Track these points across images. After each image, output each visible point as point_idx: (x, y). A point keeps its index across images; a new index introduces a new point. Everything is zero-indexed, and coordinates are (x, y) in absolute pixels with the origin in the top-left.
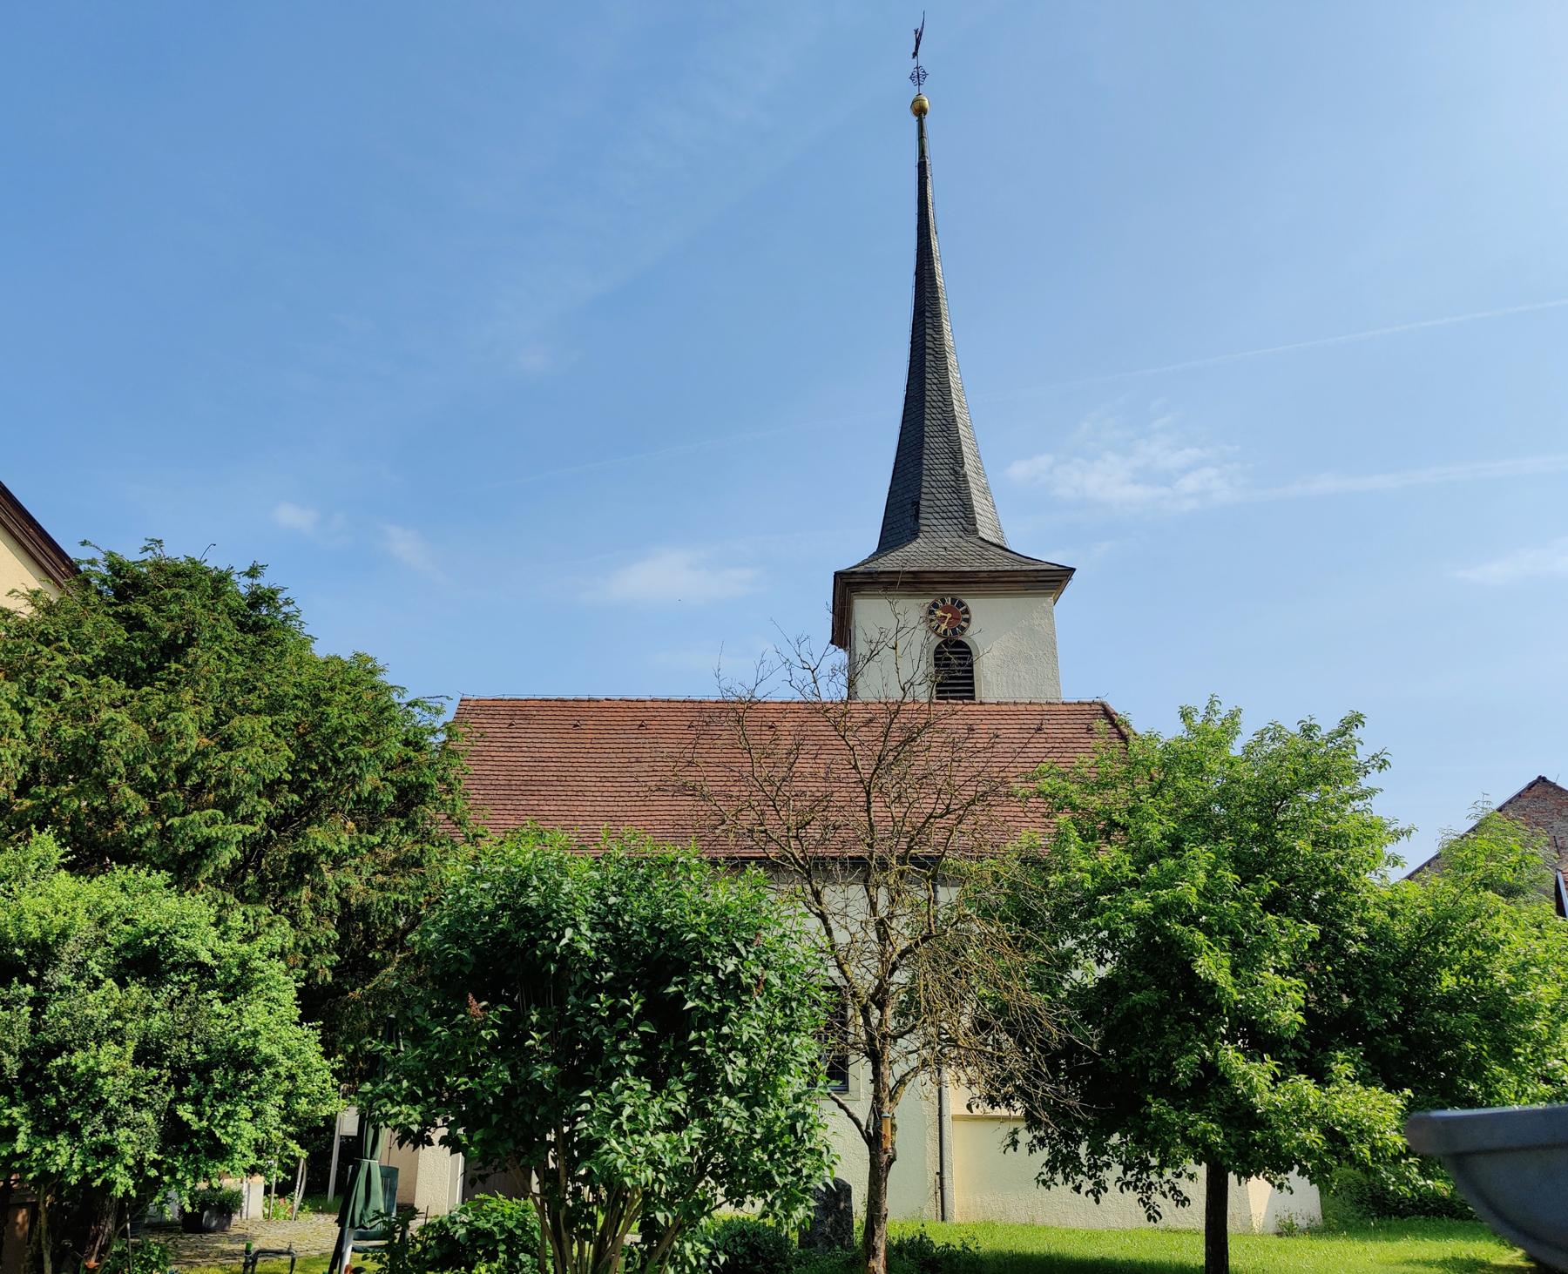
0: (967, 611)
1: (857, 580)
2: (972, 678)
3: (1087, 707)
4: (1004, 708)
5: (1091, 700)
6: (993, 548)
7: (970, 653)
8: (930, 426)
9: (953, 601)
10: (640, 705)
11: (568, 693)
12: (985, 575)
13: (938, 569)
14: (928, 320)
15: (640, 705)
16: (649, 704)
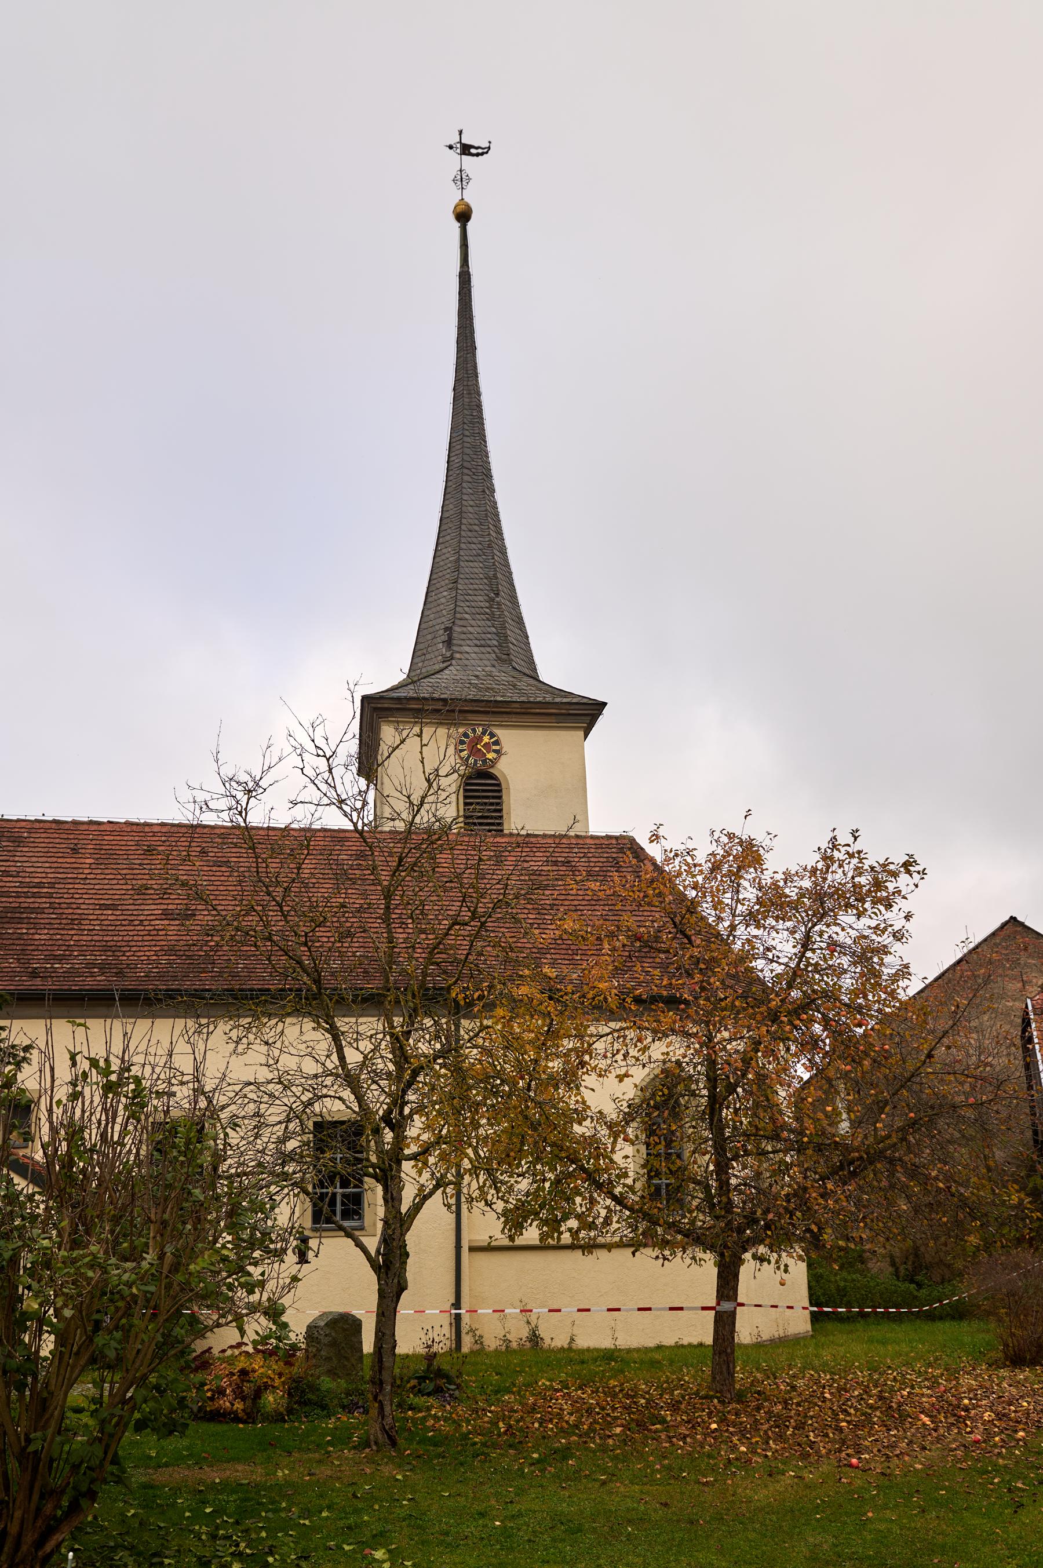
1: (386, 706)
7: (499, 785)
11: (66, 814)
12: (517, 705)
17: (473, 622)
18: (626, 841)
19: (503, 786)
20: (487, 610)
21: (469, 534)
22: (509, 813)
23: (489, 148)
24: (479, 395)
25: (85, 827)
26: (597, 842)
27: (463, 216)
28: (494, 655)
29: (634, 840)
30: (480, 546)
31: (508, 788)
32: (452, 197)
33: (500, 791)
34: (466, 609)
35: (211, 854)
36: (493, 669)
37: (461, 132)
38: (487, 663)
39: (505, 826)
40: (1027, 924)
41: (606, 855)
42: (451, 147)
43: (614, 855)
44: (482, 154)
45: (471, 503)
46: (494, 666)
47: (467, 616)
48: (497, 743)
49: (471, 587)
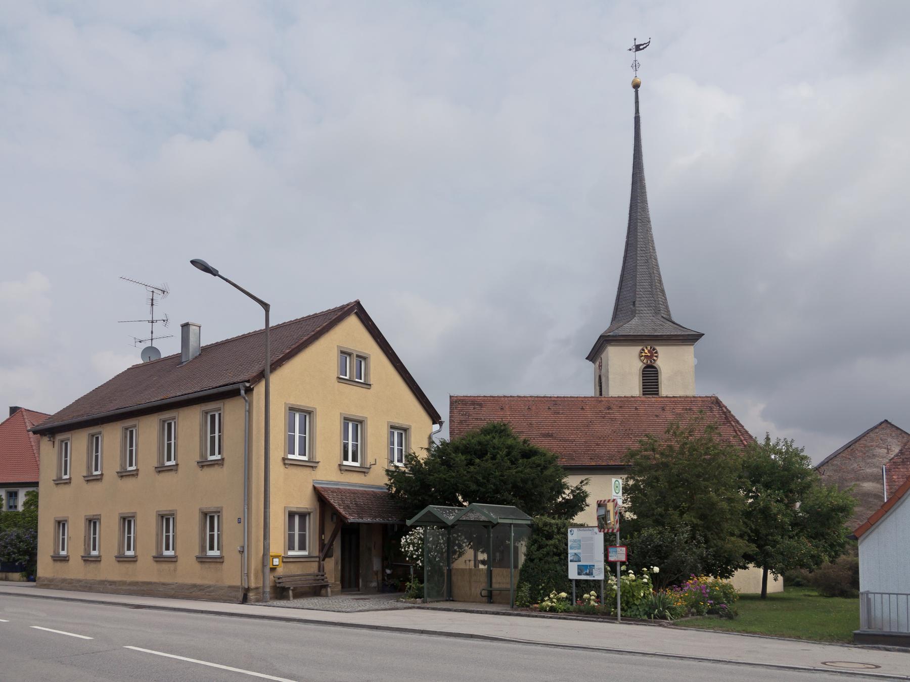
7: (657, 371)
23: (649, 42)
24: (649, 222)
27: (636, 86)
29: (718, 398)
32: (630, 77)
33: (657, 374)
36: (653, 318)
37: (635, 40)
39: (660, 394)
40: (892, 423)
41: (706, 405)
42: (630, 50)
44: (648, 45)
45: (642, 237)
48: (656, 353)
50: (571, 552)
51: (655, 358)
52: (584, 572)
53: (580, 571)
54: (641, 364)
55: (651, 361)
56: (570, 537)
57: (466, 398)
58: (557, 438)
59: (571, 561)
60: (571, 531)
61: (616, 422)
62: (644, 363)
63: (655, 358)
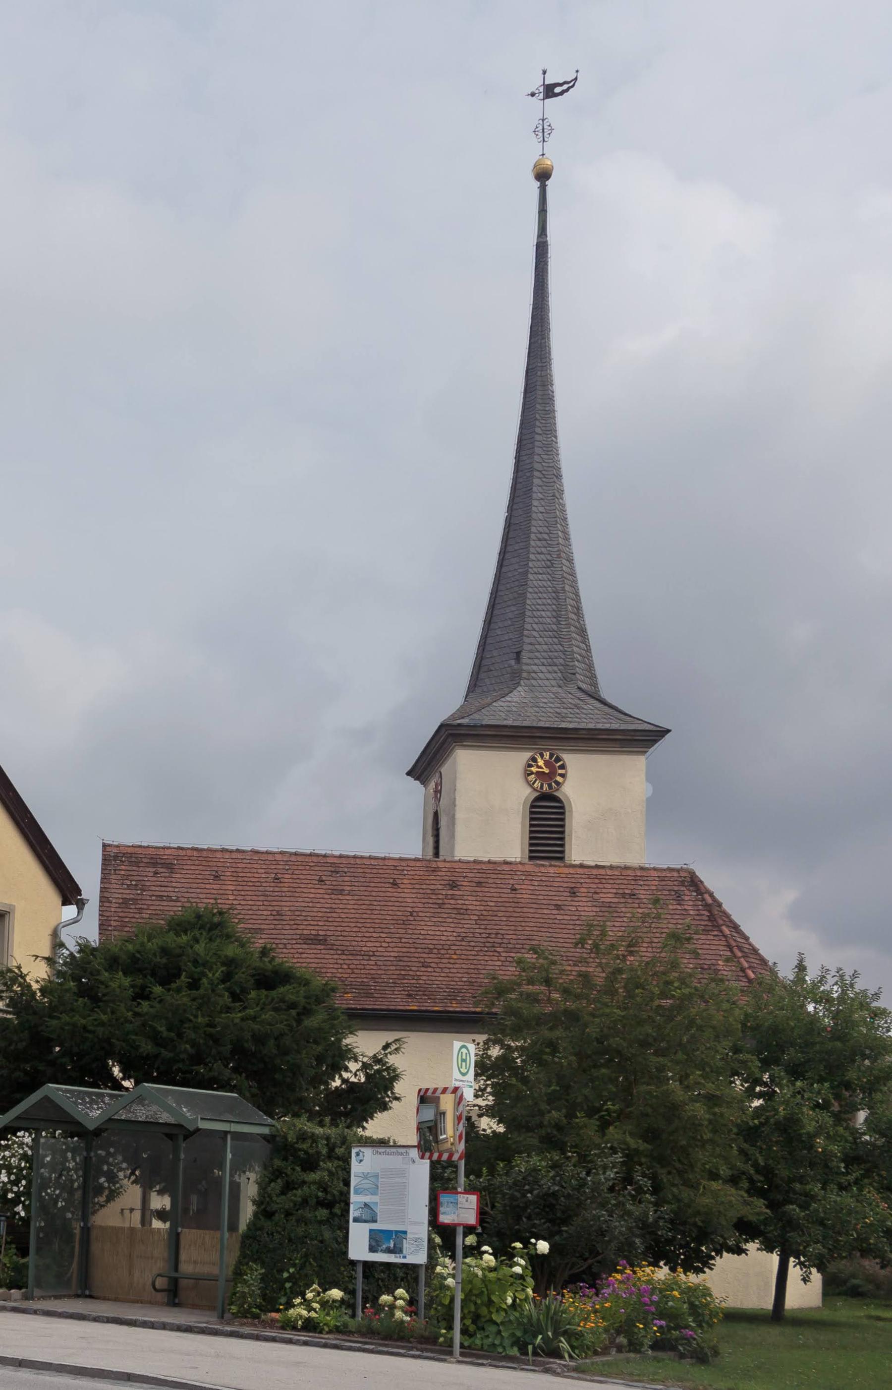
0: (563, 767)
1: (462, 732)
2: (563, 832)
3: (676, 874)
4: (602, 872)
5: (679, 867)
6: (592, 701)
7: (563, 807)
8: (536, 562)
9: (551, 756)
10: (506, 867)
11: (204, 843)
12: (584, 732)
13: (541, 724)
14: (538, 437)
15: (270, 857)
16: (279, 857)
17: (540, 640)
18: (686, 874)
19: (567, 809)
20: (554, 627)
21: (538, 543)
22: (570, 835)
23: (576, 79)
25: (219, 855)
26: (659, 874)
27: (543, 176)
28: (560, 675)
29: (694, 873)
30: (549, 557)
31: (571, 811)
33: (563, 813)
34: (535, 626)
35: (327, 883)
36: (560, 690)
37: (544, 72)
38: (554, 683)
42: (533, 95)
43: (676, 888)
45: (542, 509)
46: (560, 687)
47: (535, 633)
49: (539, 601)
50: (355, 1199)
51: (559, 779)
52: (384, 1246)
53: (374, 1244)
54: (527, 791)
55: (550, 786)
56: (356, 1168)
57: (140, 851)
58: (335, 947)
59: (356, 1220)
60: (358, 1154)
61: (466, 917)
62: (535, 790)
63: (559, 779)
